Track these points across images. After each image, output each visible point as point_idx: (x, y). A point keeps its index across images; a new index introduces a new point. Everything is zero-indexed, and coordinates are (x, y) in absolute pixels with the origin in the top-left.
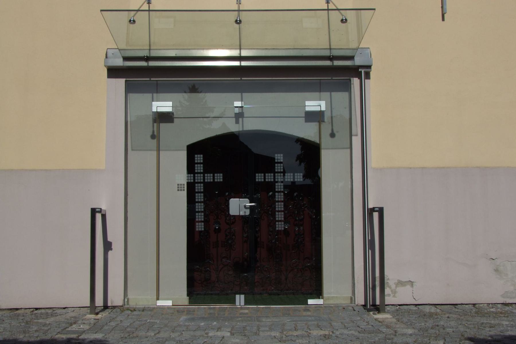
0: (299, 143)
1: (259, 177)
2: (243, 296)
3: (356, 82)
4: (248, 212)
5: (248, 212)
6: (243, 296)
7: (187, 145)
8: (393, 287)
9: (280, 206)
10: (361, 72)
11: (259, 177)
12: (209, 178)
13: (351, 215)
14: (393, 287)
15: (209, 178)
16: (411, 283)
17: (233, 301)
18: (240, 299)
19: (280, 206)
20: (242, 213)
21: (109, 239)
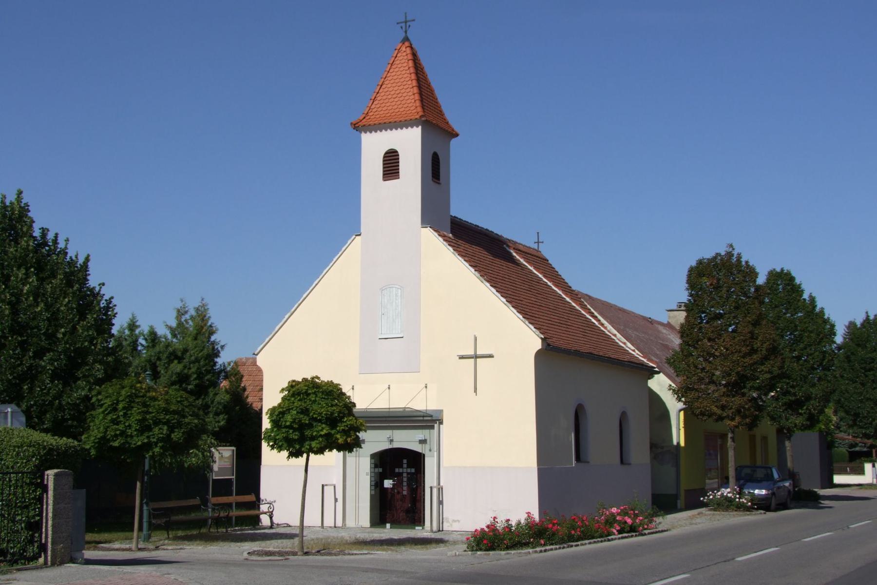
0: (290, 457)
1: (397, 470)
2: (389, 524)
3: (436, 426)
4: (391, 486)
5: (391, 486)
6: (389, 524)
7: (371, 453)
8: (451, 522)
9: (405, 484)
10: (861, 472)
11: (397, 470)
12: (405, 466)
13: (301, 513)
14: (451, 522)
15: (405, 466)
16: (459, 521)
17: (385, 527)
18: (388, 525)
19: (405, 484)
20: (389, 487)
21: (337, 497)
